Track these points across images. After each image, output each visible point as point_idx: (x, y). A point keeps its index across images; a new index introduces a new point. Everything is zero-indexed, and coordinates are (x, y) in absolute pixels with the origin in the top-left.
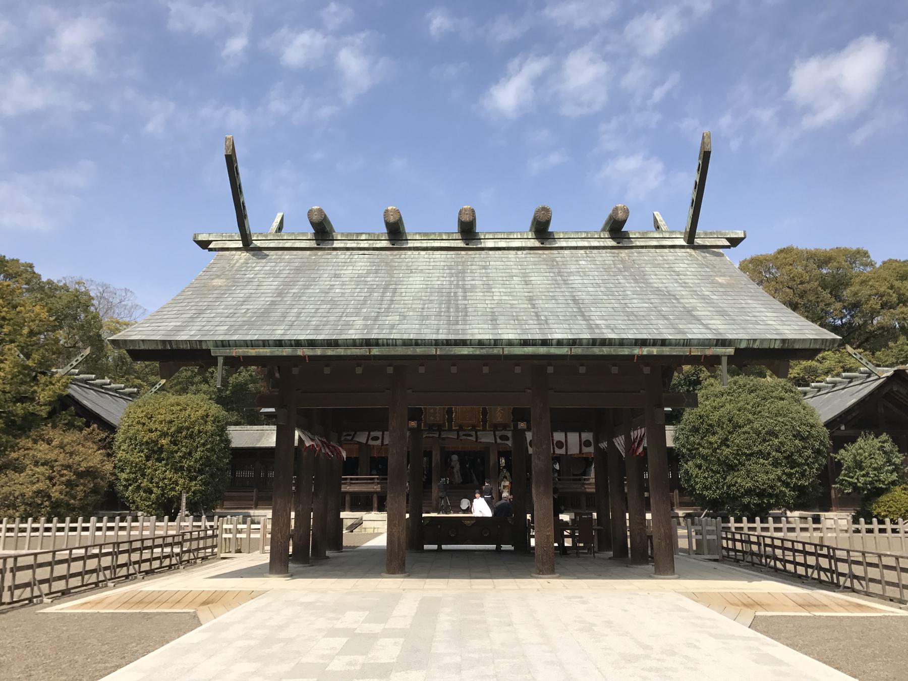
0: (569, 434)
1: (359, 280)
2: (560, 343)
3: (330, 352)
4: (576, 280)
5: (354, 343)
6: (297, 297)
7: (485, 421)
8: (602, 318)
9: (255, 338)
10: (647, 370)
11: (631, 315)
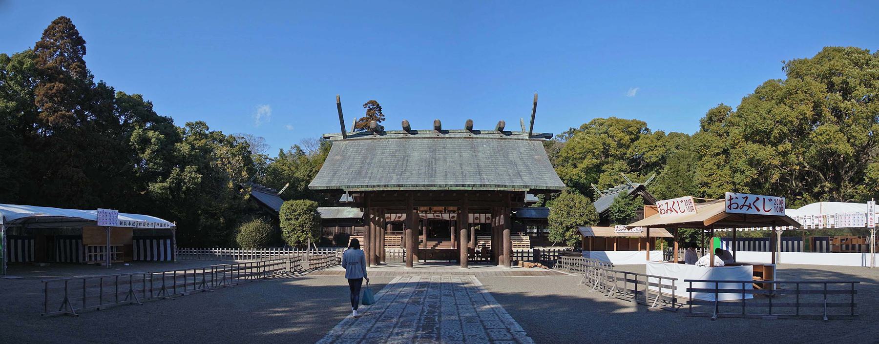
1: (393, 155)
2: (469, 185)
3: (386, 189)
6: (369, 164)
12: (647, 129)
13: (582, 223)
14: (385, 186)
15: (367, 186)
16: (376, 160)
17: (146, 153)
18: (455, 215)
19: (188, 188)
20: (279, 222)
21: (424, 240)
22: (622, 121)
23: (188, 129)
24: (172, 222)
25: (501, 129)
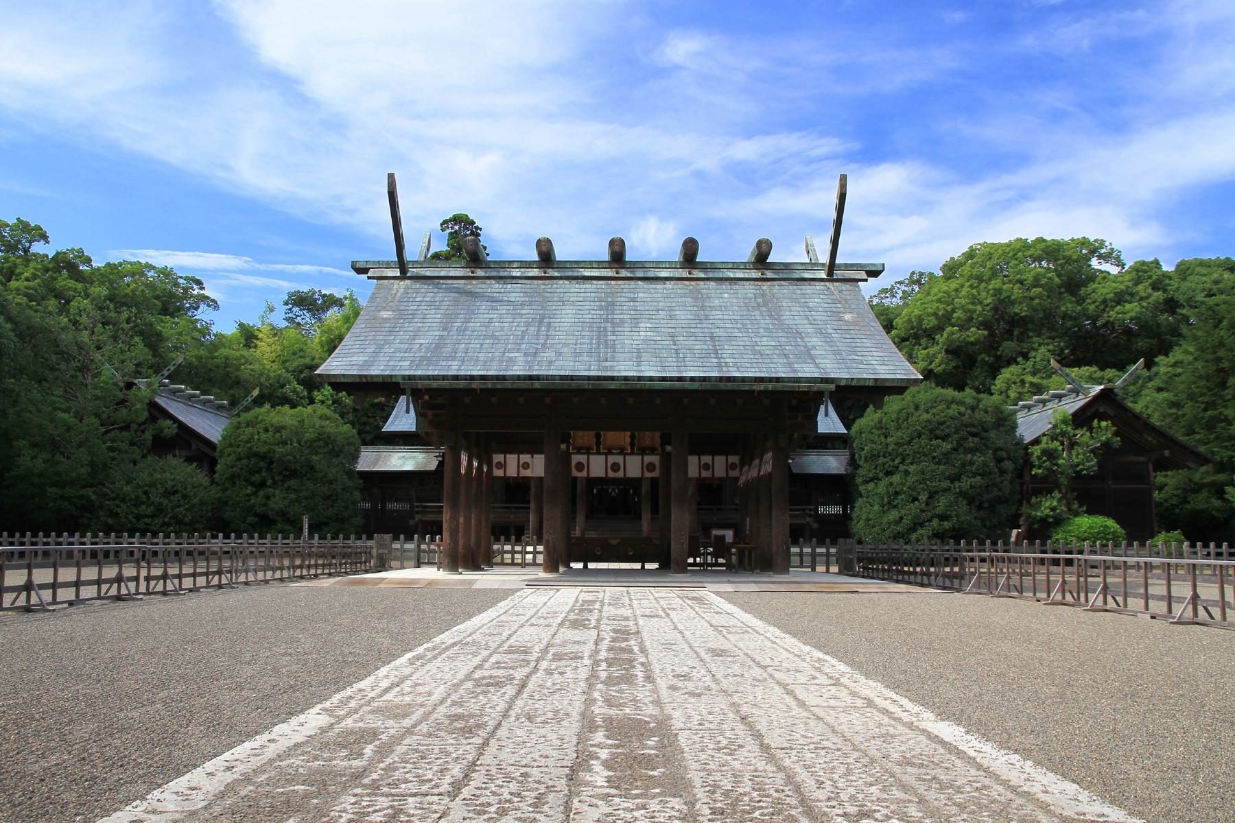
0: (716, 458)
5: (519, 378)
6: (461, 331)
7: (598, 443)
9: (436, 373)
10: (767, 402)
16: (475, 325)
18: (655, 459)
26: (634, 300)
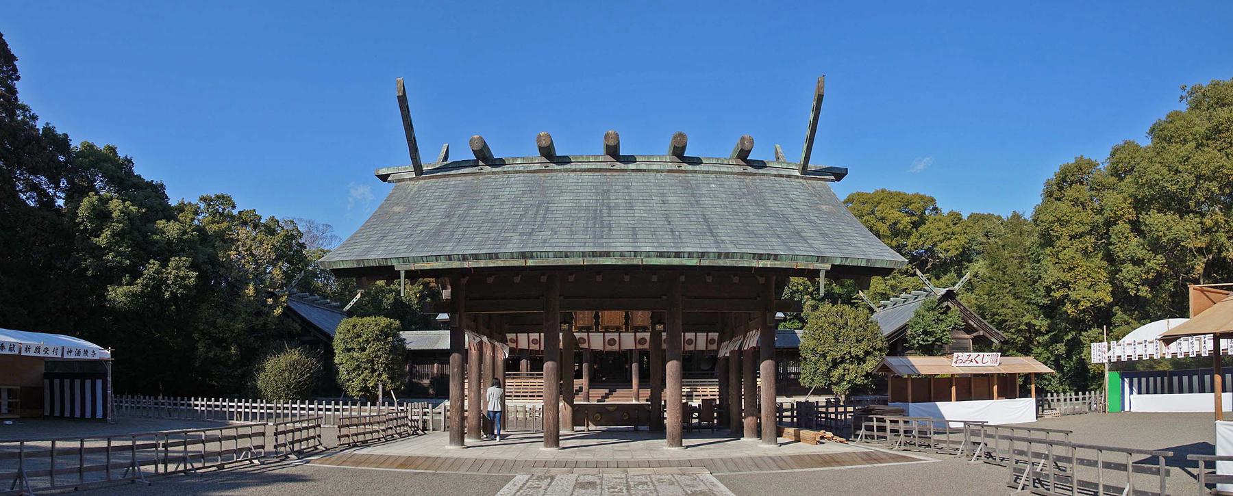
1: (516, 201)
2: (690, 255)
4: (706, 201)
5: (512, 256)
6: (463, 217)
7: (597, 324)
8: (727, 234)
11: (752, 234)
12: (935, 209)
13: (861, 354)
14: (492, 256)
15: (449, 258)
17: (103, 236)
18: (647, 335)
19: (173, 294)
20: (333, 354)
21: (585, 388)
22: (898, 194)
23: (203, 206)
24: (106, 347)
25: (743, 155)
26: (627, 188)
